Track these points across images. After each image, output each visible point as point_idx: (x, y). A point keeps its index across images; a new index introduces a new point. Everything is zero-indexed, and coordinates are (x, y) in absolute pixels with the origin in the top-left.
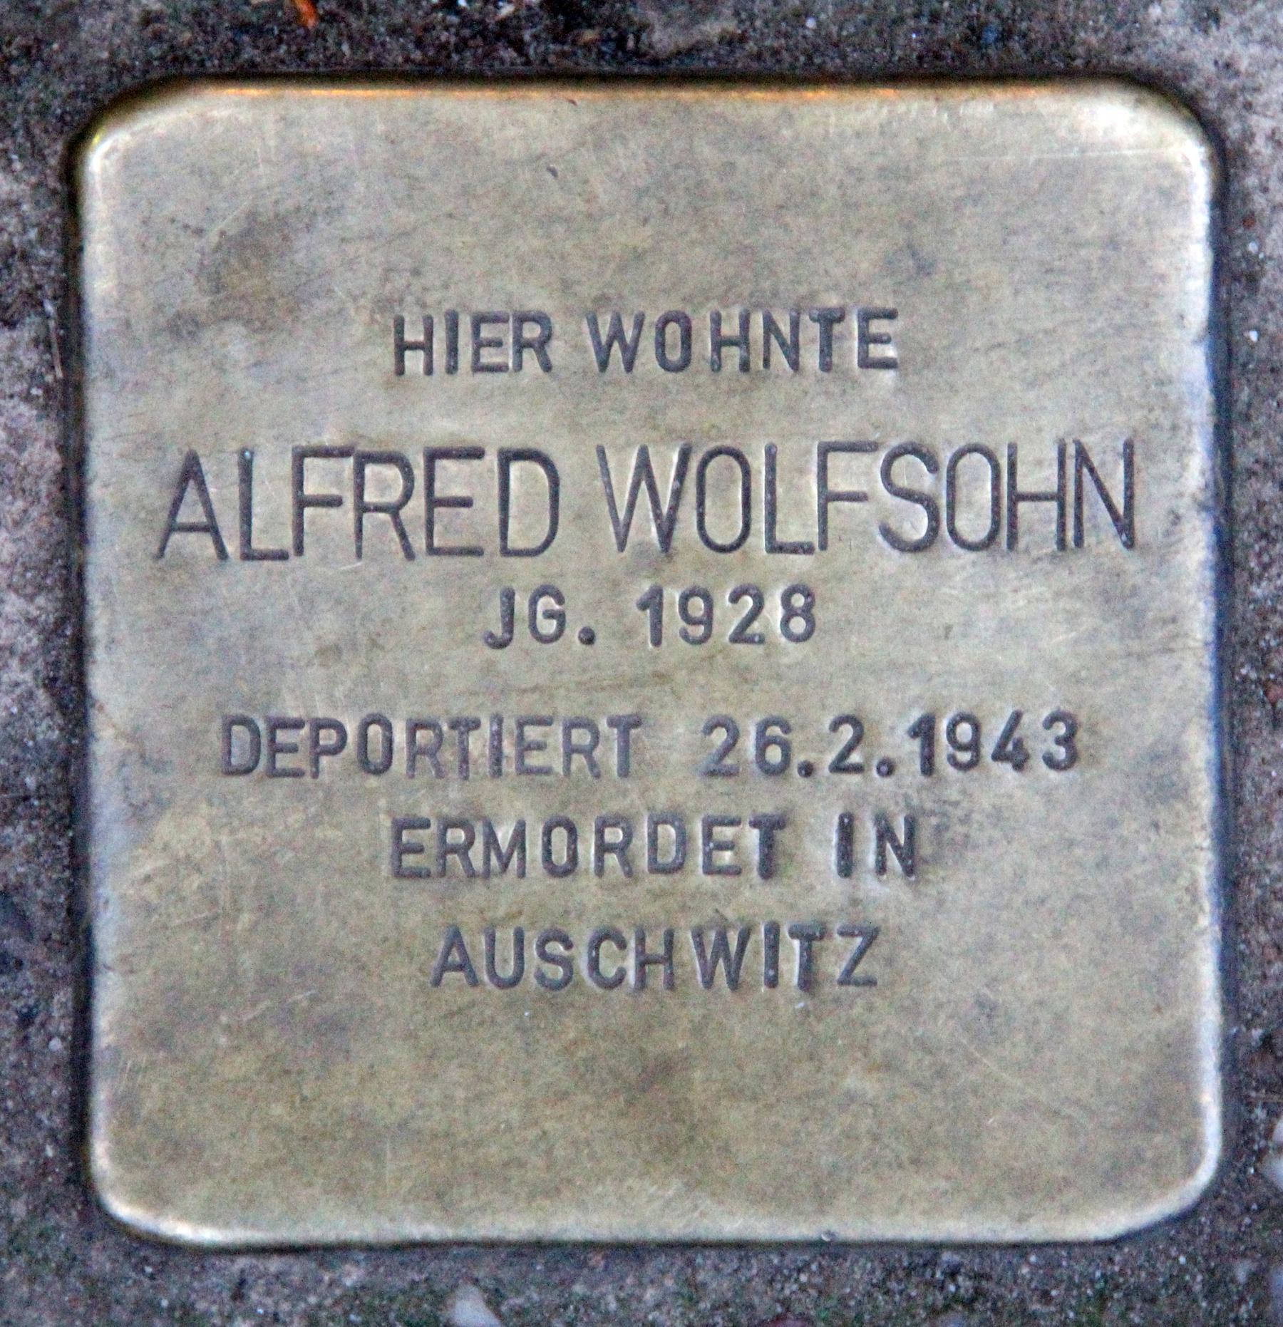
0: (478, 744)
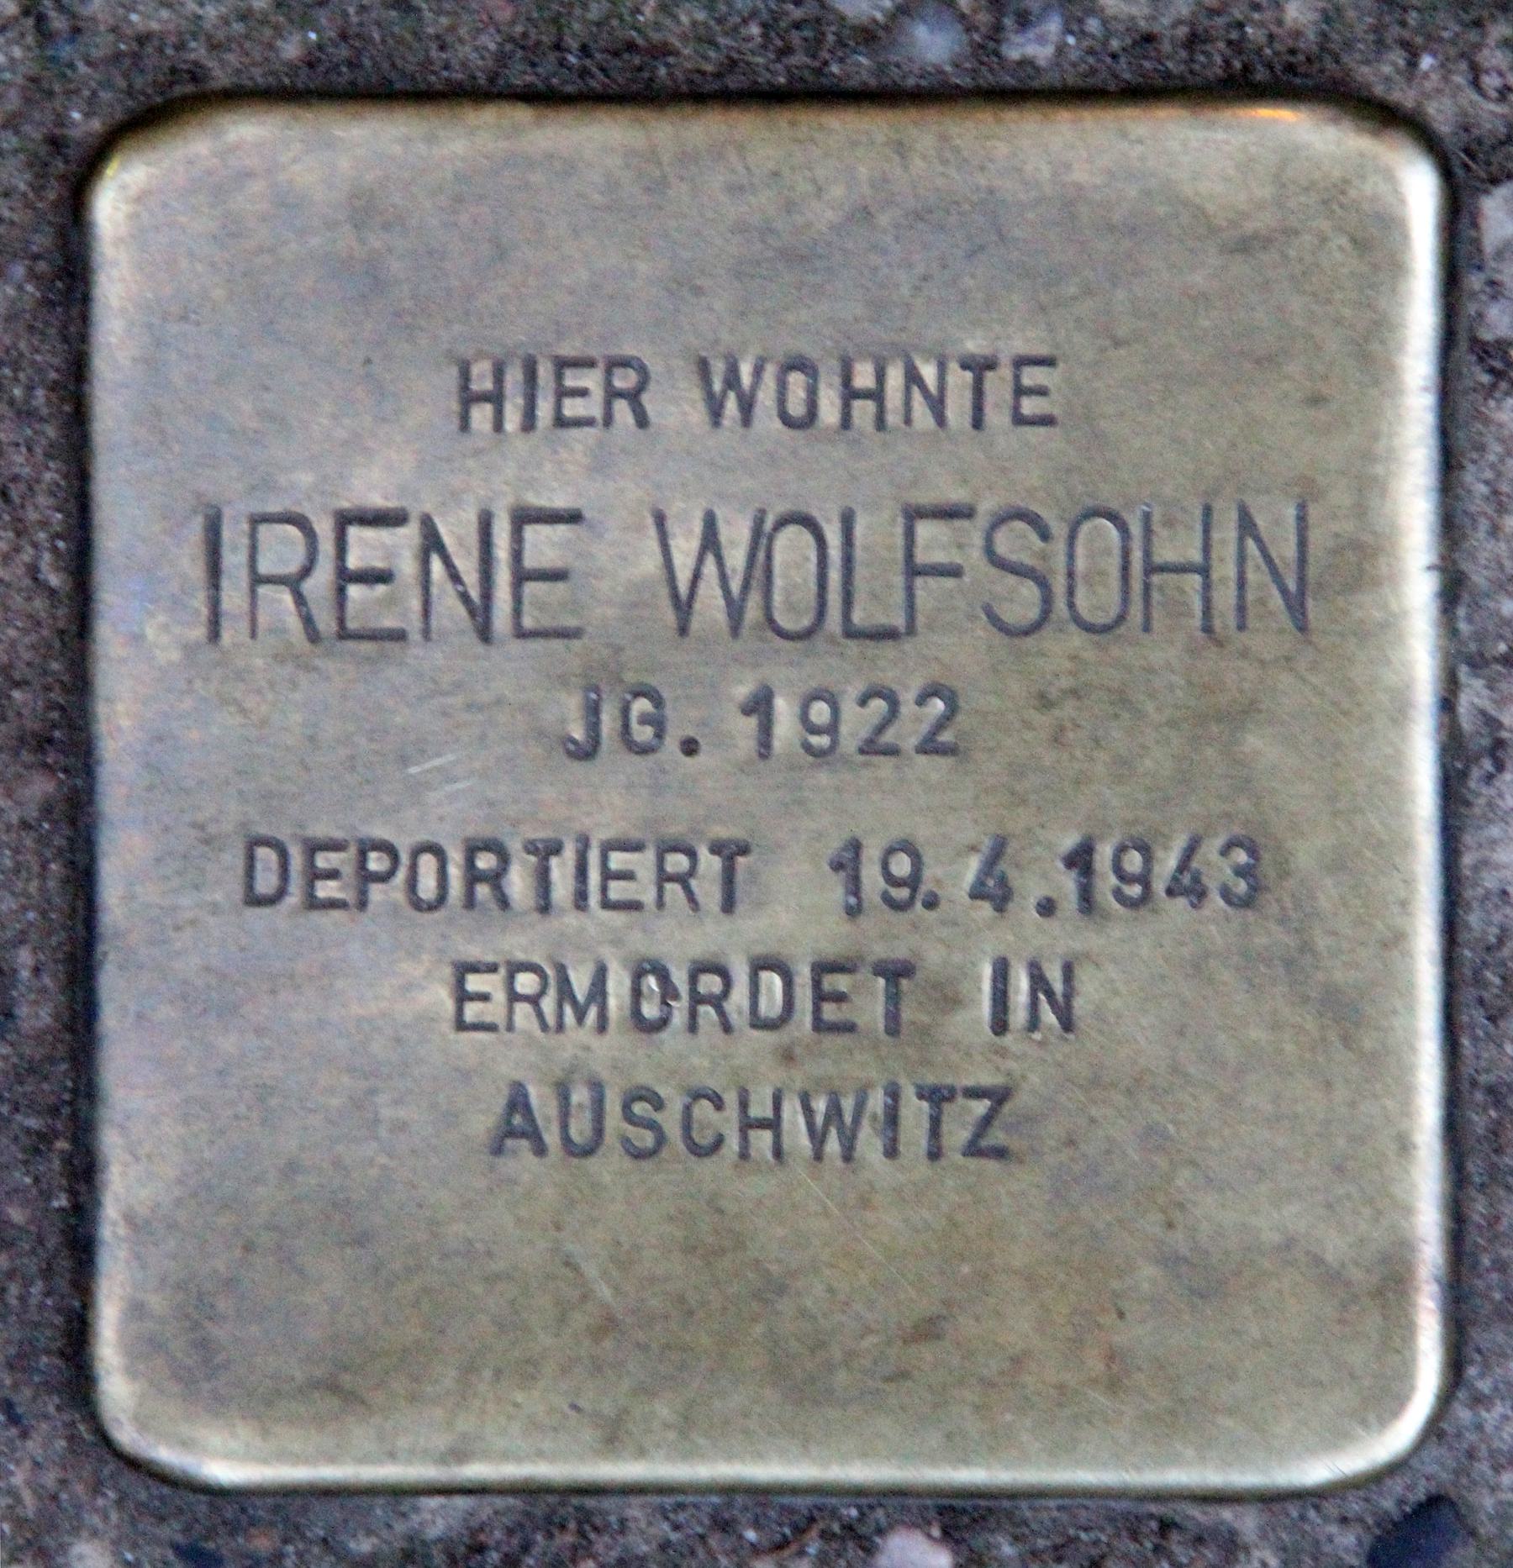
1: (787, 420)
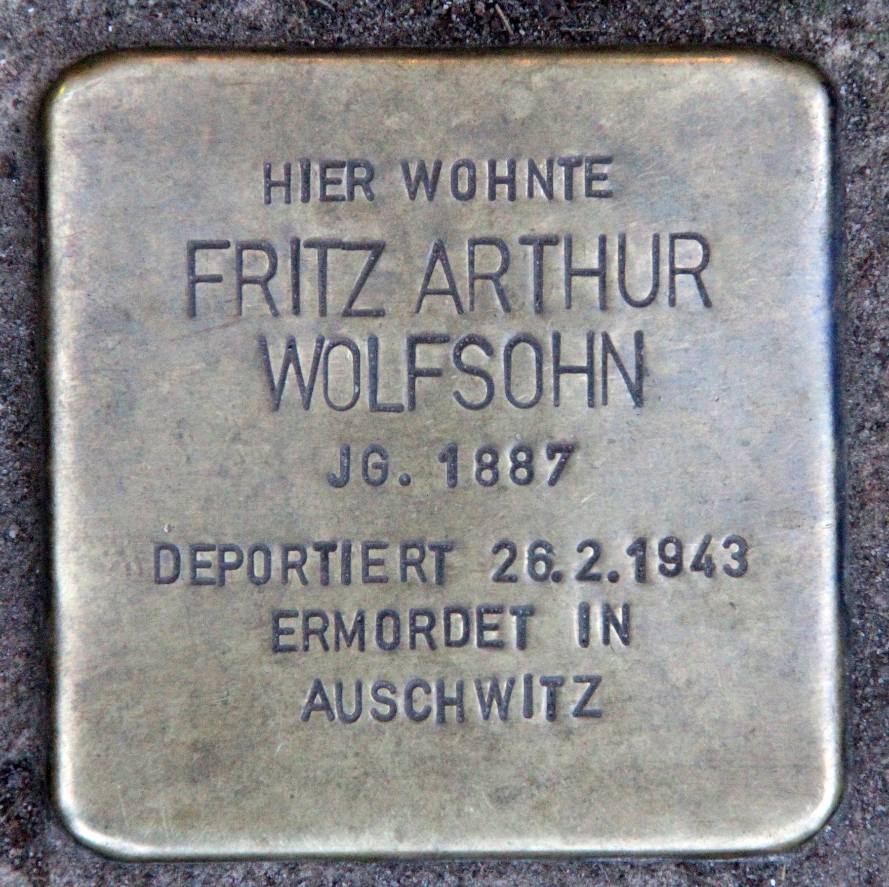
0: (335, 558)
1: (457, 195)
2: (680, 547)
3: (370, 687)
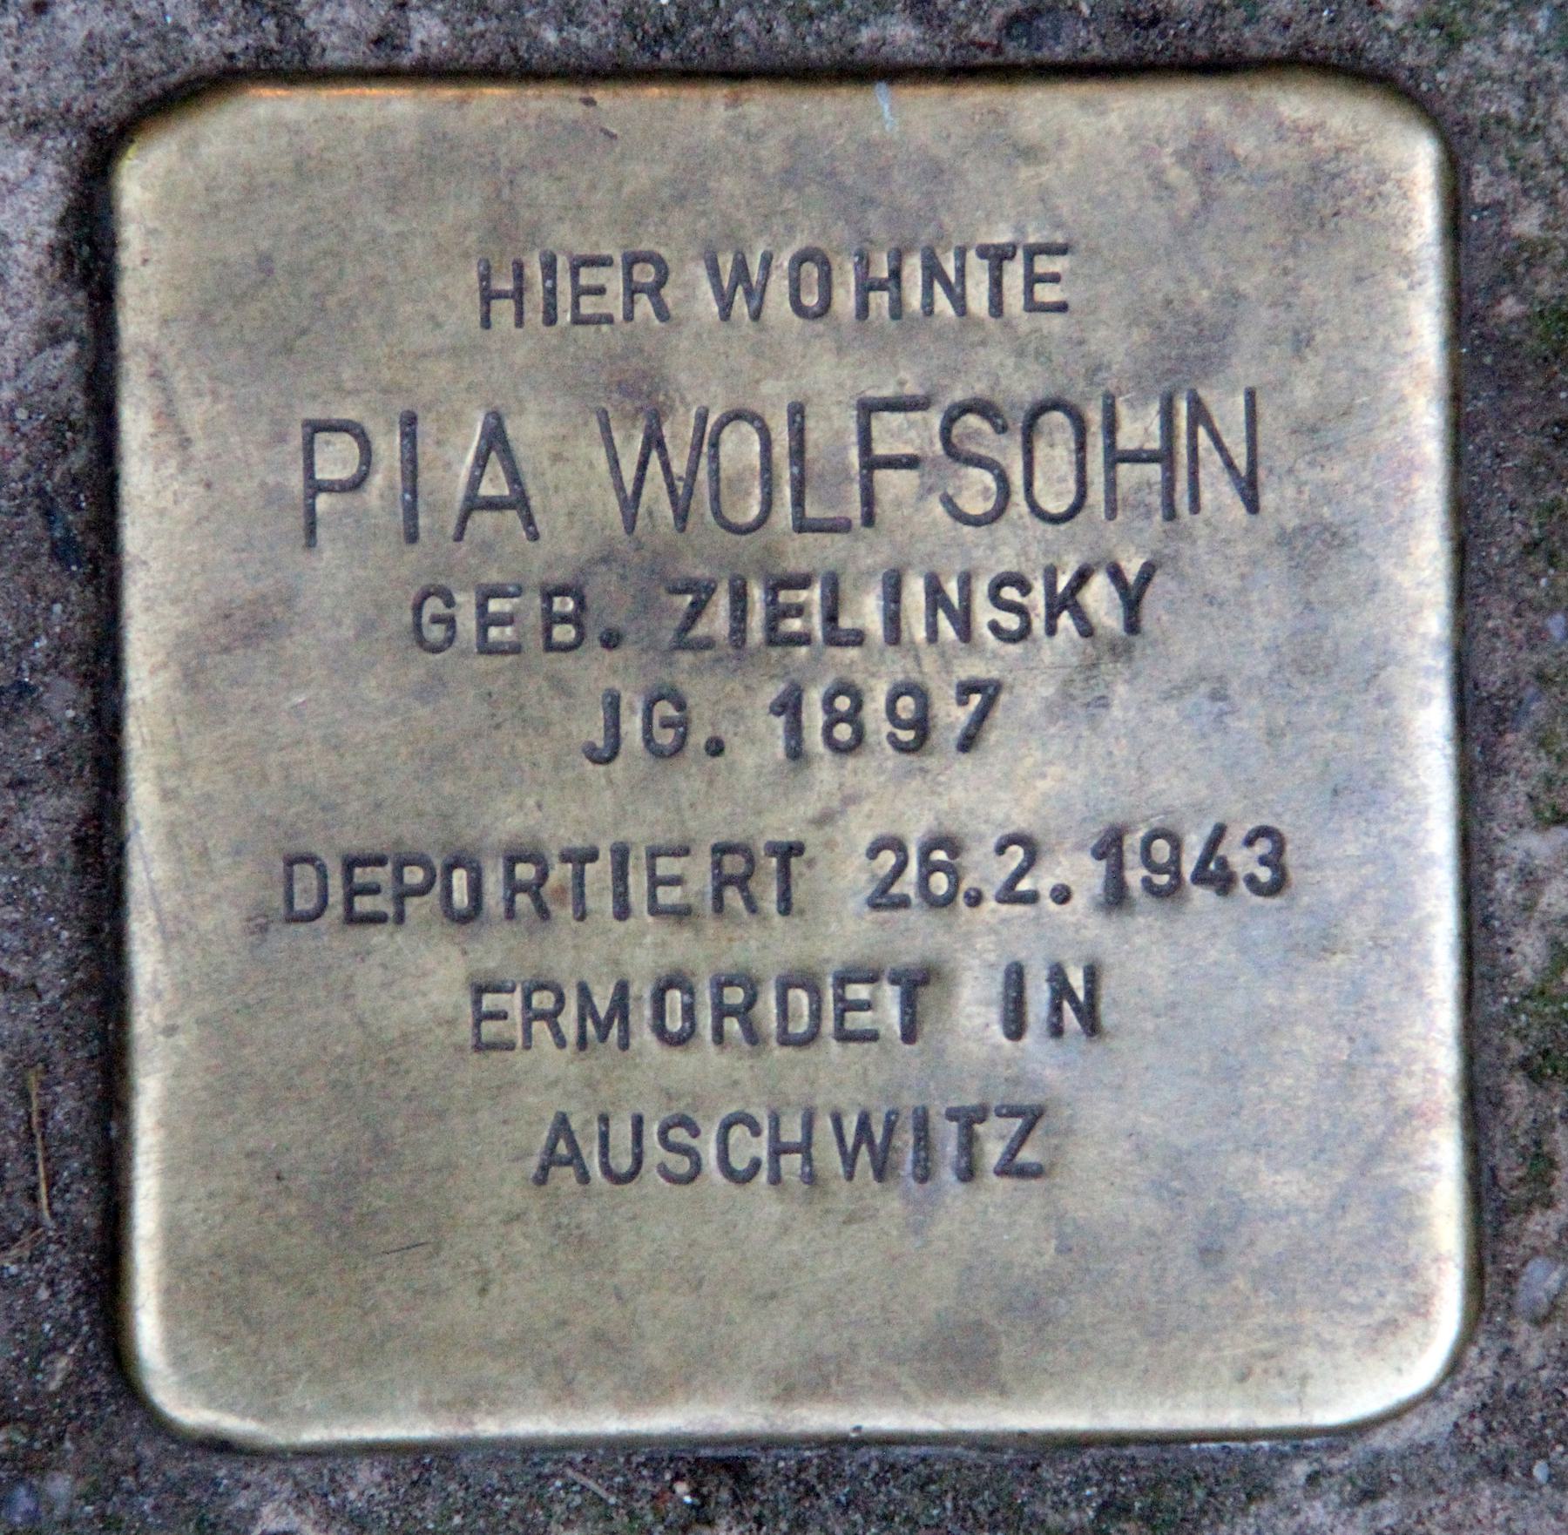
0: (599, 873)
1: (799, 308)
2: (1177, 846)
3: (655, 1128)
